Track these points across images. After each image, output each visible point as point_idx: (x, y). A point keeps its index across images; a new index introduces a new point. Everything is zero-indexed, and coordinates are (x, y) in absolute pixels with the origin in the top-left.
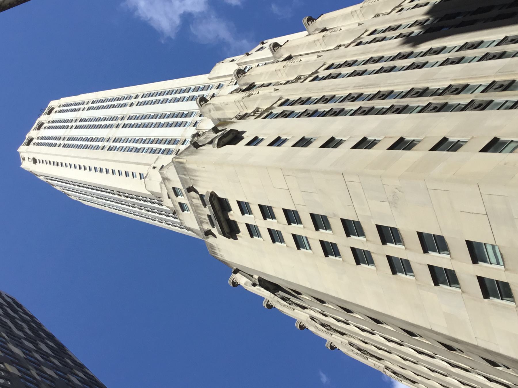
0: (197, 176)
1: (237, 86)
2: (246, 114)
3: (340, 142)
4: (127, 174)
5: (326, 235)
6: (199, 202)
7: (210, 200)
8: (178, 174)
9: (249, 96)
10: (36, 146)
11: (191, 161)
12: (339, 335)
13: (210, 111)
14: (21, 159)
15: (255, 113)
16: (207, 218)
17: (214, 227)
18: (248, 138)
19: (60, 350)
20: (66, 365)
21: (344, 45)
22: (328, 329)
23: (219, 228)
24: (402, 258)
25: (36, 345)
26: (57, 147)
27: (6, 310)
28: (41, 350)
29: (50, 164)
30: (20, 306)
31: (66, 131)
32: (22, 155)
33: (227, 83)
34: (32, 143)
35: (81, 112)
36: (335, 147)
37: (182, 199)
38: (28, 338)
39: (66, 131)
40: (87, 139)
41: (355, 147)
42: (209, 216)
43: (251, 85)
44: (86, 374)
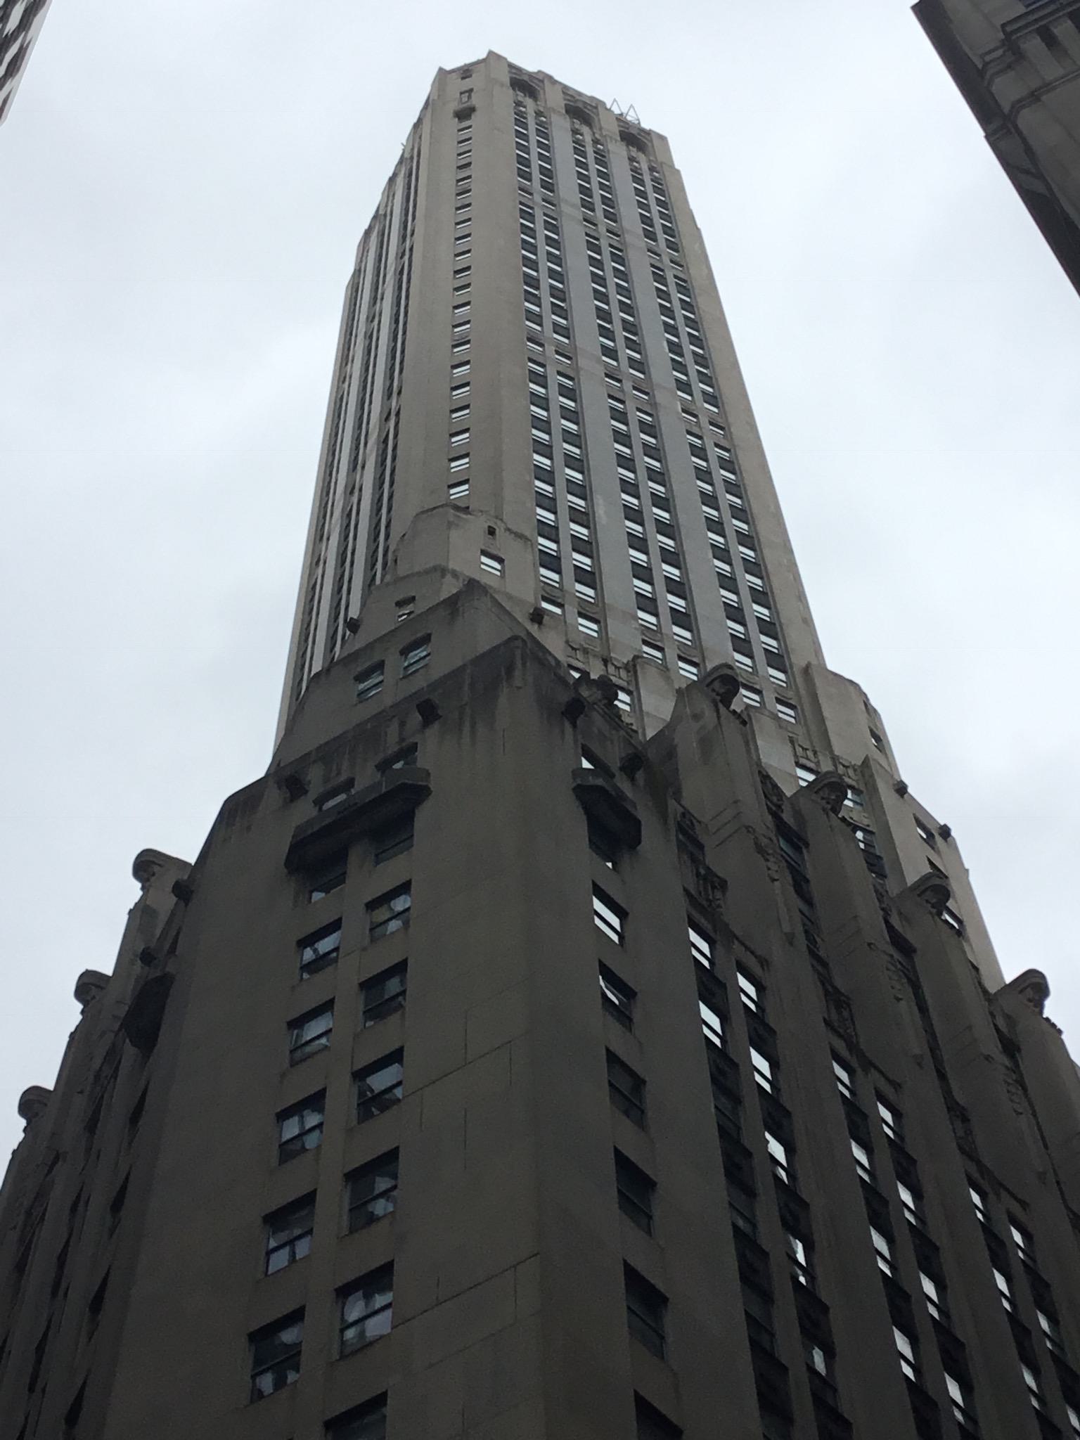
2: (701, 847)
6: (392, 743)
9: (760, 850)
13: (696, 717)
15: (705, 879)
16: (343, 778)
21: (968, 1132)
23: (316, 828)
24: (415, 838)
27: (16, 39)
31: (573, 206)
39: (573, 206)
41: (631, 1273)
43: (800, 839)
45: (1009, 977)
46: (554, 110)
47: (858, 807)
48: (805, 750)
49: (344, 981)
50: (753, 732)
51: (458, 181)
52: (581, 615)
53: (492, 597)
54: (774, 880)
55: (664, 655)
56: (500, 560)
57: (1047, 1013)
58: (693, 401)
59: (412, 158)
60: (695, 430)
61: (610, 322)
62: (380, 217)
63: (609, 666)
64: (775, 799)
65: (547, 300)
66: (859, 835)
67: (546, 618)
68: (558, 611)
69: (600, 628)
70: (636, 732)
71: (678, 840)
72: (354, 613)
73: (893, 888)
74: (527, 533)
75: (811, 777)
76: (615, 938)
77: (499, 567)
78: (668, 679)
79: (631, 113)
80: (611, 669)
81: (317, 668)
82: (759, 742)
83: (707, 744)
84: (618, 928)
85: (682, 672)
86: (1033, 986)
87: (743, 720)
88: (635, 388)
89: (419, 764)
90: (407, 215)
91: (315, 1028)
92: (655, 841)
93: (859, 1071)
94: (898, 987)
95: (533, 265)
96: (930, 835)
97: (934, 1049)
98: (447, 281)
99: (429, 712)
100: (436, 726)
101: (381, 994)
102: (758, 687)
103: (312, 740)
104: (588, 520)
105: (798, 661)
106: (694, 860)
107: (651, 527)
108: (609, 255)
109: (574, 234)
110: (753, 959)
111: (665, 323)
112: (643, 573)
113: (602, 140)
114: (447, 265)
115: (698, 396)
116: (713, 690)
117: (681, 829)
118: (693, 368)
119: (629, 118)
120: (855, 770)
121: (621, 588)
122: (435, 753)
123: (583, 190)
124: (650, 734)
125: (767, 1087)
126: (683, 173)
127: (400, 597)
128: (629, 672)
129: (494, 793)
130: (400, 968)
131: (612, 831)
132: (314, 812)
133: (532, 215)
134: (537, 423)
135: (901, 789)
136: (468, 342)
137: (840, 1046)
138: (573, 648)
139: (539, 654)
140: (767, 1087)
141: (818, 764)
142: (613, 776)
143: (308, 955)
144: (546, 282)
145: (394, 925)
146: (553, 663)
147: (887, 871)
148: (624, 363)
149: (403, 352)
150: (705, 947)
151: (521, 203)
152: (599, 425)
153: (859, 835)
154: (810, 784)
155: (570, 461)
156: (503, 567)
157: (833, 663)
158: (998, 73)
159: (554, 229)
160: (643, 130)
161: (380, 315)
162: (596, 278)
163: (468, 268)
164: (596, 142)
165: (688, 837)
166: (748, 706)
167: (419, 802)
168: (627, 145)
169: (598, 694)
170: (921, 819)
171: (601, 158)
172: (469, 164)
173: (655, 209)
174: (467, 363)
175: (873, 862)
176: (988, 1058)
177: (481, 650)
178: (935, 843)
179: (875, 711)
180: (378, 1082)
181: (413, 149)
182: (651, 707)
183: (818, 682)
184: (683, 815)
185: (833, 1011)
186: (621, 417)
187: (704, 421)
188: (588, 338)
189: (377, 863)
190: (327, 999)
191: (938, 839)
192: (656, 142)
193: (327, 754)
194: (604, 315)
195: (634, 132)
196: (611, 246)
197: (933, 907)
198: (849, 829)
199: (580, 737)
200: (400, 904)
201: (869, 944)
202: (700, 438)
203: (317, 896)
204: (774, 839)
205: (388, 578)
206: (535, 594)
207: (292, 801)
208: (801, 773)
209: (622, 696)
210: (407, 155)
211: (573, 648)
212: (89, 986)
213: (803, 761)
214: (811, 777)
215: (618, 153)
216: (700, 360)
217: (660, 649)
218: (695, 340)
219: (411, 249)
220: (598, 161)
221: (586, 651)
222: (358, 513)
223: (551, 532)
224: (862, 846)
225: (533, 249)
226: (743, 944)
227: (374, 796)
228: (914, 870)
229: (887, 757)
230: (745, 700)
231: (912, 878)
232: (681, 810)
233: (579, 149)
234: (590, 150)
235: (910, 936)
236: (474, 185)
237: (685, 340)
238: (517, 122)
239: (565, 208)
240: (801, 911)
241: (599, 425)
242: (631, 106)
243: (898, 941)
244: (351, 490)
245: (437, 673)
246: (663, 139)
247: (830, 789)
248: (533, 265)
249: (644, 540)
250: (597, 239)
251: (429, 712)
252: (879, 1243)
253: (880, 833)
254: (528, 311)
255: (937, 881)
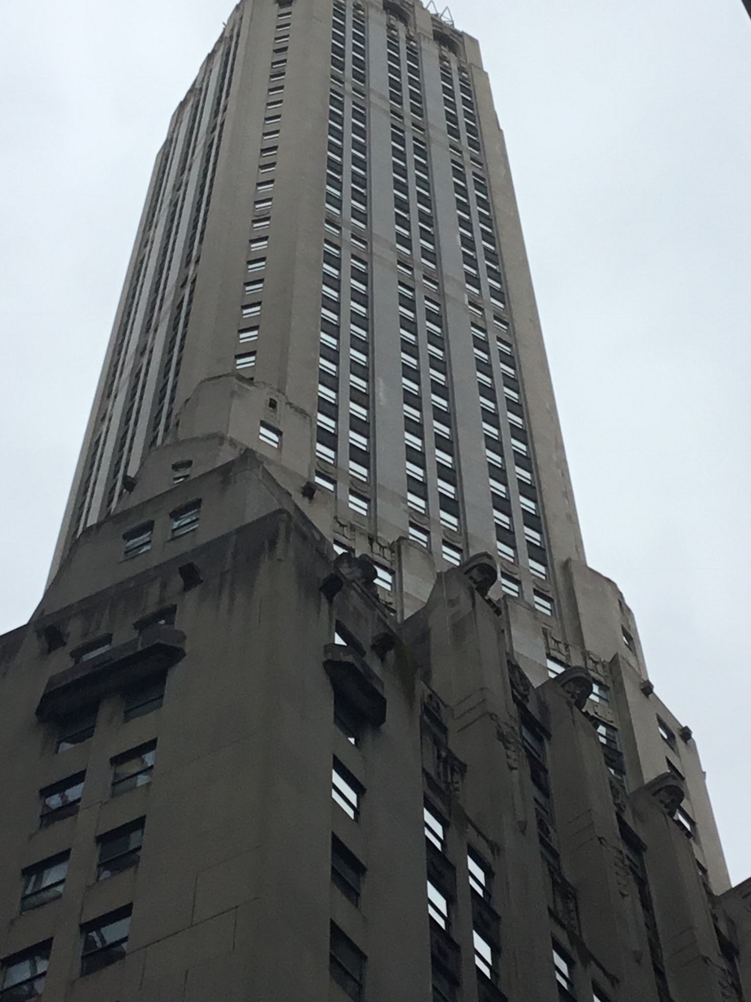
0: (232, 598)
2: (444, 730)
6: (151, 606)
7: (159, 648)
9: (501, 737)
11: (278, 579)
13: (452, 603)
15: (445, 762)
16: (102, 632)
24: (165, 699)
31: (381, 97)
39: (381, 97)
42: (108, 639)
43: (543, 729)
45: (735, 882)
46: (372, 6)
47: (603, 702)
48: (557, 642)
49: (82, 834)
50: (508, 623)
51: (273, 64)
52: (352, 493)
53: (265, 471)
54: (512, 768)
55: (429, 539)
56: (279, 433)
58: (480, 295)
59: (231, 37)
60: (481, 324)
61: (407, 211)
62: (196, 91)
63: (375, 544)
64: (521, 688)
65: (348, 185)
66: (602, 730)
67: (317, 494)
68: (330, 487)
69: (369, 507)
70: (394, 611)
71: (422, 720)
73: (631, 786)
74: (308, 409)
75: (560, 670)
76: (351, 813)
77: (276, 438)
78: (432, 564)
79: (446, 14)
80: (376, 548)
81: (93, 520)
82: (513, 632)
83: (459, 629)
84: (355, 803)
85: (445, 556)
87: (498, 609)
88: (425, 278)
89: (176, 626)
90: (221, 91)
91: (51, 876)
92: (399, 722)
93: (579, 965)
94: (624, 882)
95: (339, 151)
96: (671, 735)
98: (253, 157)
100: (195, 592)
101: (118, 849)
102: (516, 577)
103: (79, 590)
104: (445, 368)
105: (559, 556)
106: (436, 742)
107: (428, 413)
108: (412, 146)
109: (380, 126)
110: (484, 842)
111: (460, 218)
112: (416, 457)
113: (416, 39)
114: (255, 141)
115: (486, 290)
116: (471, 578)
117: (426, 710)
118: (483, 263)
119: (443, 19)
120: (604, 666)
121: (396, 469)
122: (194, 618)
123: (393, 83)
124: (408, 614)
125: (486, 971)
126: (490, 76)
127: (177, 459)
128: (393, 552)
129: (250, 657)
130: (139, 824)
131: (358, 708)
132: (71, 664)
133: (342, 103)
134: (328, 303)
135: (647, 689)
136: (268, 219)
137: (564, 939)
138: (341, 525)
139: (304, 531)
140: (486, 971)
141: (568, 657)
142: (363, 654)
143: (55, 801)
144: (349, 168)
145: (142, 780)
146: (318, 538)
147: (627, 768)
148: (417, 251)
149: (205, 221)
150: (438, 829)
151: (332, 90)
152: (388, 308)
153: (602, 730)
154: (559, 676)
155: (356, 343)
156: (280, 440)
157: (593, 561)
159: (362, 118)
160: (455, 32)
161: (186, 185)
162: (397, 168)
163: (275, 148)
164: (409, 38)
165: (433, 721)
166: (506, 596)
168: (440, 44)
169: (358, 573)
170: (664, 719)
171: (413, 55)
172: (285, 49)
173: (460, 107)
174: (266, 238)
175: (612, 756)
176: (705, 960)
177: (249, 520)
178: (675, 742)
179: (629, 610)
180: (112, 933)
181: (232, 30)
182: (407, 588)
184: (430, 696)
185: (558, 900)
186: (410, 304)
187: (489, 315)
188: (384, 225)
189: (127, 720)
190: (65, 849)
191: (678, 739)
192: (467, 42)
193: (88, 608)
194: (402, 205)
195: (448, 33)
196: (415, 139)
197: (666, 806)
198: (590, 724)
199: (335, 613)
200: (149, 758)
201: (600, 839)
202: (484, 331)
203: (66, 746)
204: (517, 728)
205: (167, 442)
206: (310, 471)
207: (49, 651)
208: (551, 665)
209: (381, 573)
210: (227, 35)
211: (341, 525)
213: (554, 653)
214: (560, 670)
215: (430, 52)
216: (490, 256)
217: (426, 532)
218: (487, 237)
219: (222, 125)
220: (409, 58)
221: (353, 528)
222: (146, 374)
223: (331, 410)
224: (603, 740)
225: (339, 135)
226: (475, 827)
227: (131, 653)
228: (652, 767)
229: (636, 655)
230: (504, 589)
231: (649, 776)
232: (429, 692)
233: (392, 44)
234: (403, 46)
235: (642, 833)
236: (289, 68)
237: (478, 236)
238: (336, 13)
239: (373, 98)
240: (536, 800)
241: (388, 308)
242: (447, 8)
243: (627, 835)
244: (142, 351)
245: (203, 538)
246: (475, 42)
247: (576, 683)
248: (339, 151)
249: (420, 425)
250: (402, 132)
251: (190, 576)
253: (622, 730)
254: (329, 194)
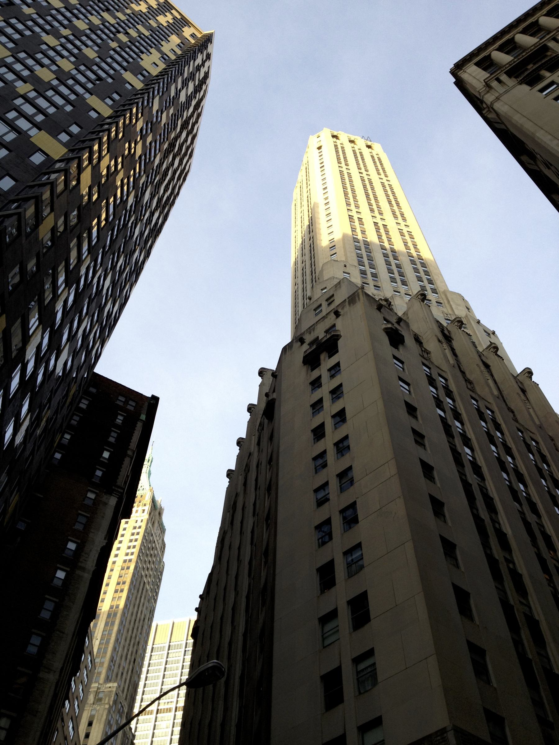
1: (445, 324)
3: (423, 445)
4: (326, 199)
5: (331, 456)
8: (348, 298)
10: (333, 144)
12: (243, 482)
14: (318, 134)
17: (308, 344)
18: (401, 353)
19: (156, 231)
20: (146, 242)
22: (245, 470)
25: (156, 209)
26: (337, 165)
28: (153, 216)
29: (321, 163)
30: (184, 180)
32: (321, 133)
33: (445, 310)
34: (335, 139)
35: (378, 176)
36: (416, 442)
37: (325, 309)
38: (160, 200)
40: (353, 191)
44: (143, 262)
49: (324, 392)
57: (533, 380)
72: (309, 294)
73: (480, 350)
76: (408, 392)
86: (529, 373)
97: (165, 694)
99: (337, 314)
135: (479, 322)
158: (485, 94)
165: (417, 340)
167: (338, 339)
183: (448, 295)
191: (492, 335)
212: (251, 408)
252: (493, 448)
255: (493, 345)
